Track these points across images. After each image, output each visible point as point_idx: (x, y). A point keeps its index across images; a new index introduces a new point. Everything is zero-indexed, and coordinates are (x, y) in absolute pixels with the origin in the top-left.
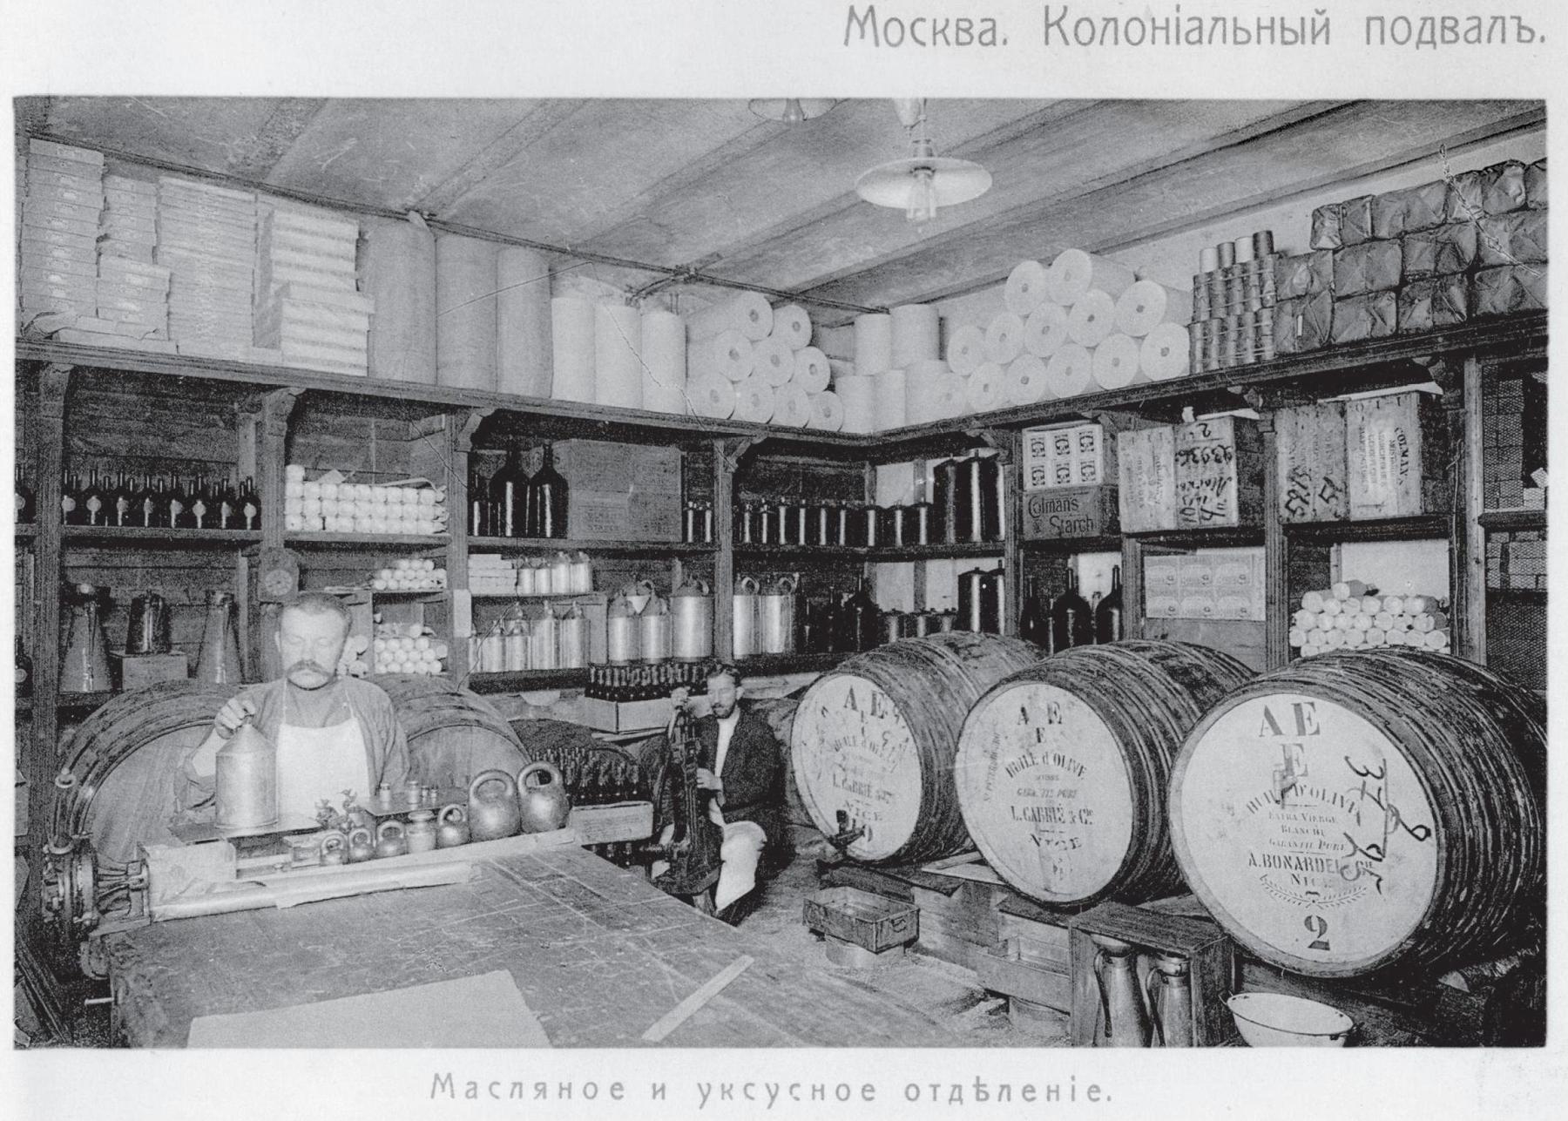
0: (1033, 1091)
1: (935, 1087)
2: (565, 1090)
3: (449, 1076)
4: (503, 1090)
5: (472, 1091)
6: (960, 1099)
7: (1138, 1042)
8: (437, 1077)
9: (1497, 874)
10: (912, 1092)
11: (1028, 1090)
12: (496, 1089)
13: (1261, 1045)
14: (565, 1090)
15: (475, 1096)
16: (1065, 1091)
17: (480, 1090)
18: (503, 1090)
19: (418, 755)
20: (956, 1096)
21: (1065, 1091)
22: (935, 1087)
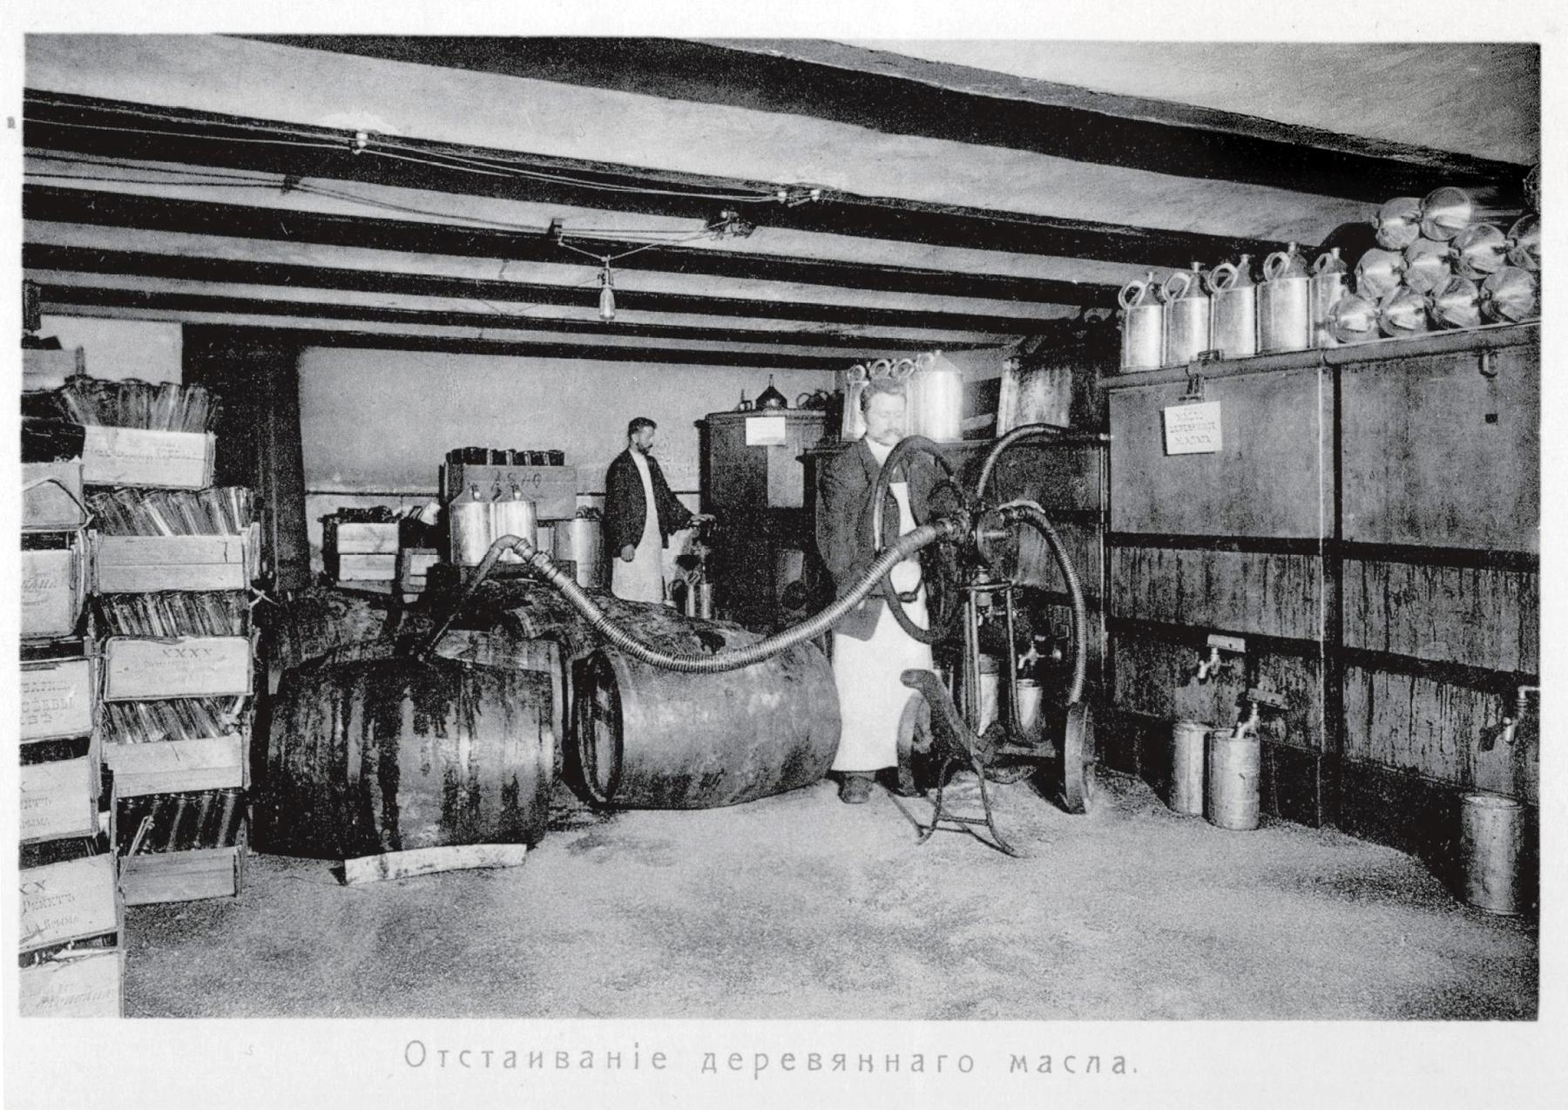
0: (793, 1059)
1: (487, 1054)
2: (892, 1062)
3: (540, 1056)
4: (1079, 1065)
5: (1047, 1065)
6: (714, 1068)
7: (117, 1010)
8: (1015, 1059)
9: (1044, 434)
10: (709, 1062)
11: (787, 1058)
12: (1070, 1063)
13: (23, 981)
14: (892, 1062)
15: (1049, 1070)
16: (628, 1059)
17: (1053, 1066)
18: (1079, 1065)
19: (970, 960)
20: (709, 1064)
21: (628, 1059)
22: (487, 1054)
